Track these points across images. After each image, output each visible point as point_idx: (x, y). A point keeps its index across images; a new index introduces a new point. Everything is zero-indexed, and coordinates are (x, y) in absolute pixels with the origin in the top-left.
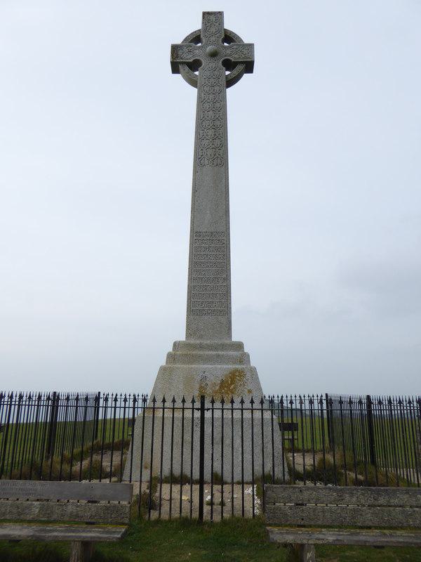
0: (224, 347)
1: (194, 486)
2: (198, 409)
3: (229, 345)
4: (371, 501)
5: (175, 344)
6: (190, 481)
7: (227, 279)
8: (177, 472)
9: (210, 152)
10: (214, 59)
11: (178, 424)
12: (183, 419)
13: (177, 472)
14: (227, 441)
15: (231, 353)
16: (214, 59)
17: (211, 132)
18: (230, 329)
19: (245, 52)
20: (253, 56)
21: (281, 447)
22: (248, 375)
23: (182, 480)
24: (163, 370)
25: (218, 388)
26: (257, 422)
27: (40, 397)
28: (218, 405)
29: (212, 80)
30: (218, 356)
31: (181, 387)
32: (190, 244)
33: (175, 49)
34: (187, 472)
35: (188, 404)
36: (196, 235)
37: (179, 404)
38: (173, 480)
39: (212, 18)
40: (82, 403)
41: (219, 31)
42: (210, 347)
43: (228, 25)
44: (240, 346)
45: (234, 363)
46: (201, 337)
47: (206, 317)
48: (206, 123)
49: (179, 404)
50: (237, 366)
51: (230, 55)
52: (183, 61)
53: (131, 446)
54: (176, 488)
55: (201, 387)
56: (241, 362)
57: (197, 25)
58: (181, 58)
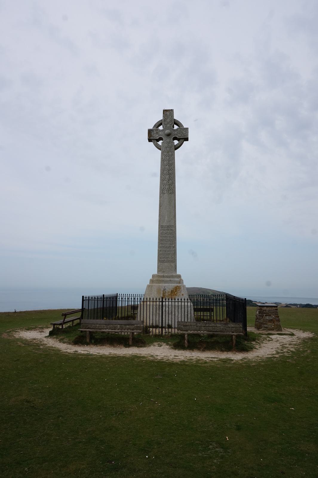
0: (172, 277)
1: (160, 329)
2: (161, 302)
3: (175, 276)
4: (204, 325)
5: (153, 276)
6: (160, 328)
7: (175, 247)
8: (154, 324)
9: (167, 187)
10: (169, 134)
11: (155, 307)
12: (156, 305)
13: (154, 324)
14: (173, 313)
15: (176, 279)
16: (169, 134)
17: (167, 176)
18: (176, 268)
19: (184, 132)
20: (188, 135)
21: (193, 315)
22: (182, 288)
23: (156, 327)
24: (148, 286)
25: (170, 293)
26: (183, 307)
27: (89, 297)
28: (170, 300)
29: (168, 149)
30: (170, 280)
31: (156, 293)
32: (159, 231)
33: (150, 131)
34: (158, 324)
35: (158, 300)
36: (161, 227)
37: (155, 300)
38: (153, 327)
39: (168, 113)
40: (112, 299)
41: (171, 121)
42: (167, 277)
43: (176, 117)
44: (179, 276)
45: (177, 283)
46: (164, 272)
47: (166, 264)
48: (165, 172)
49: (155, 300)
50: (178, 285)
51: (177, 135)
52: (153, 136)
53: (136, 318)
54: (154, 329)
55: (163, 293)
56: (179, 283)
57: (160, 117)
58: (153, 137)
